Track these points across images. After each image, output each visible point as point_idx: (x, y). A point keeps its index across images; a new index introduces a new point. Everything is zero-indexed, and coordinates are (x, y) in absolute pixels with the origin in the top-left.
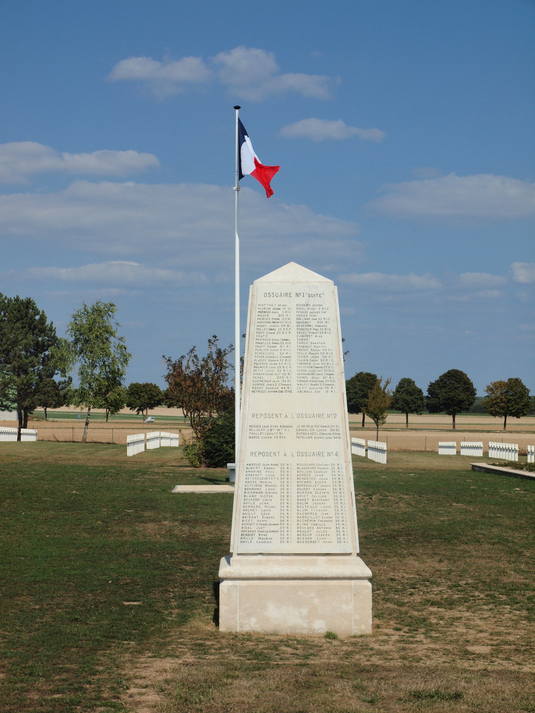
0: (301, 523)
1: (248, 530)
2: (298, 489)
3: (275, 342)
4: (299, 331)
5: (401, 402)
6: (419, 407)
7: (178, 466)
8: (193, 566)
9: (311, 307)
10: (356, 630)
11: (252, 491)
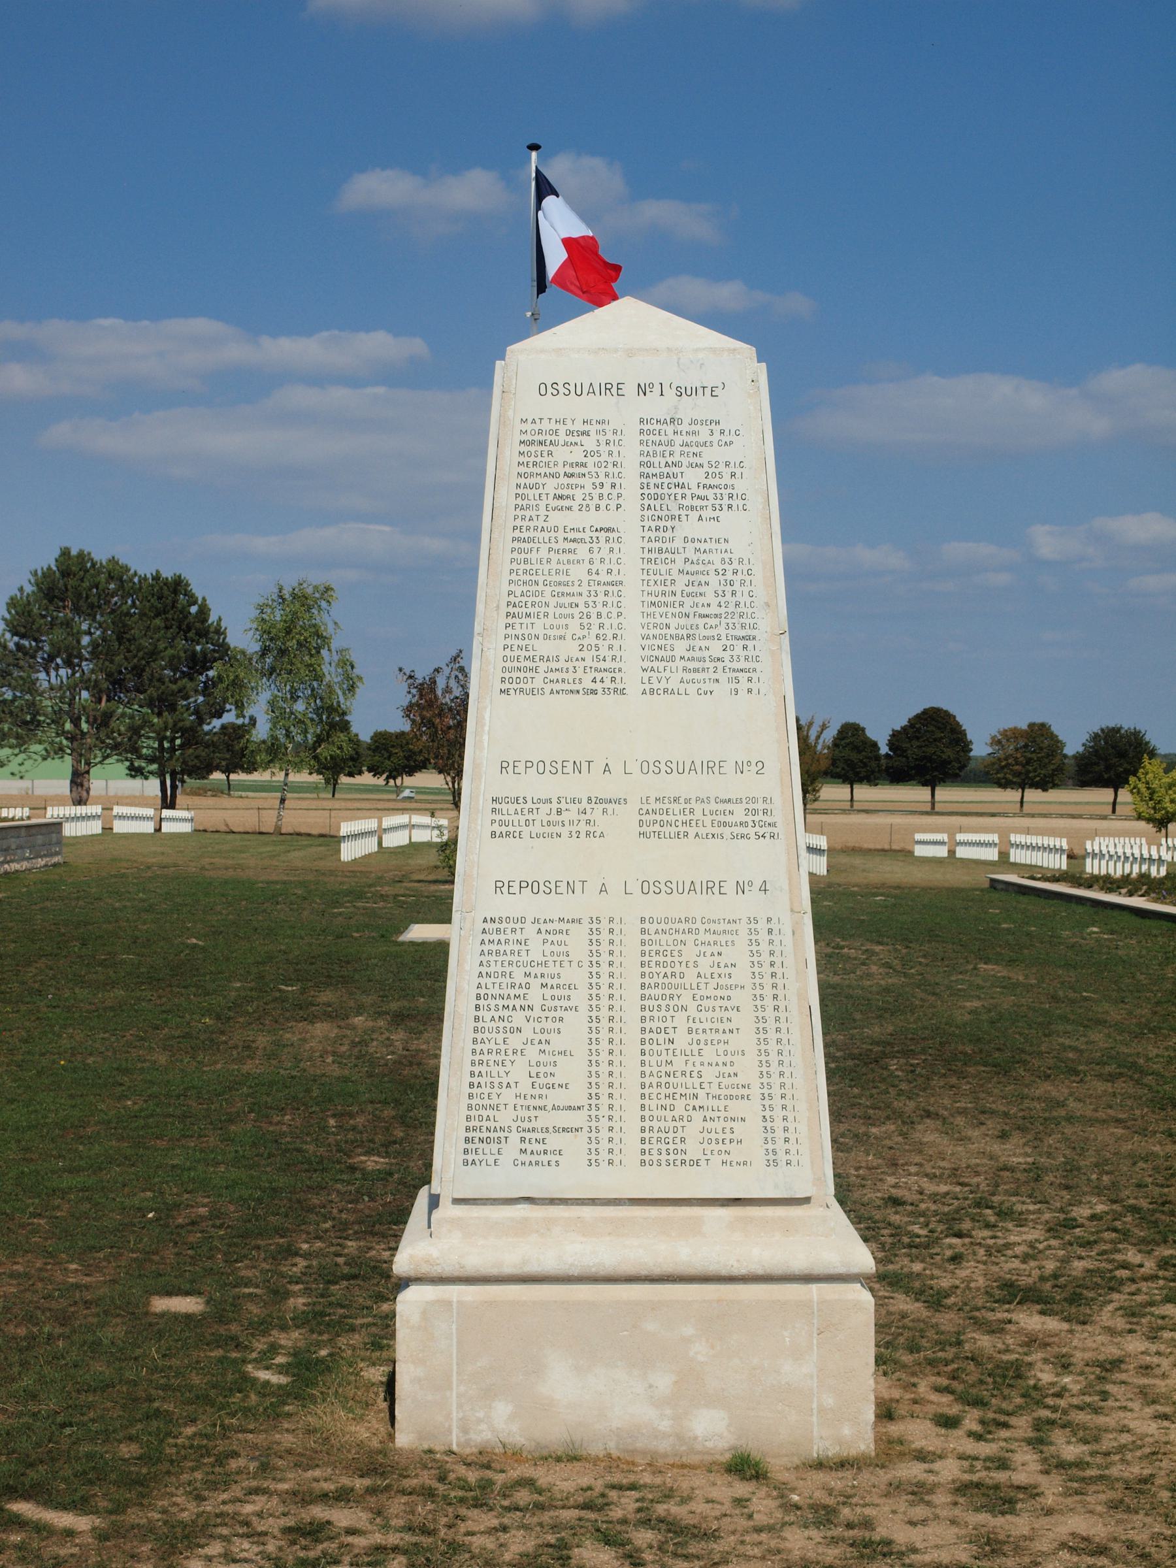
0: (653, 1103)
1: (485, 1124)
2: (643, 997)
3: (571, 536)
4: (646, 502)
5: (841, 765)
6: (873, 772)
7: (430, 882)
8: (388, 1155)
9: (685, 427)
10: (823, 1445)
11: (501, 1003)
